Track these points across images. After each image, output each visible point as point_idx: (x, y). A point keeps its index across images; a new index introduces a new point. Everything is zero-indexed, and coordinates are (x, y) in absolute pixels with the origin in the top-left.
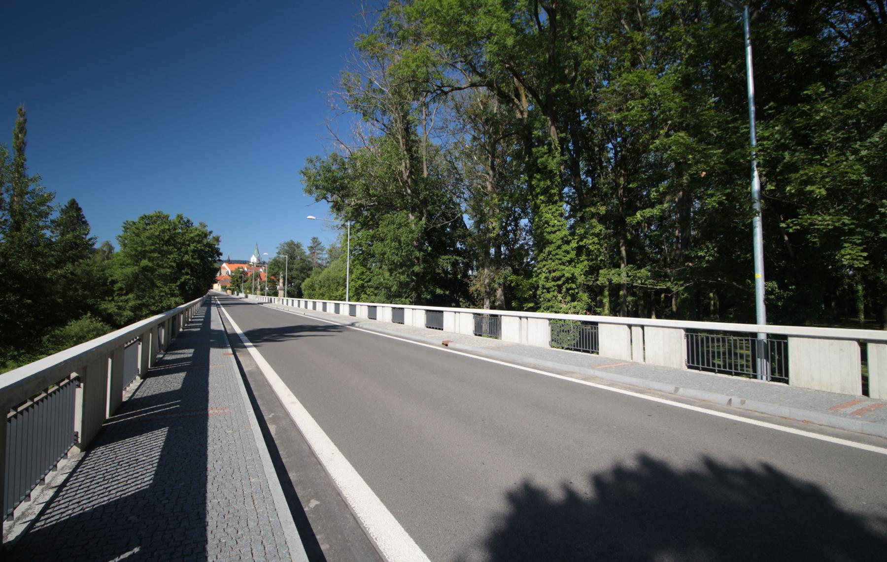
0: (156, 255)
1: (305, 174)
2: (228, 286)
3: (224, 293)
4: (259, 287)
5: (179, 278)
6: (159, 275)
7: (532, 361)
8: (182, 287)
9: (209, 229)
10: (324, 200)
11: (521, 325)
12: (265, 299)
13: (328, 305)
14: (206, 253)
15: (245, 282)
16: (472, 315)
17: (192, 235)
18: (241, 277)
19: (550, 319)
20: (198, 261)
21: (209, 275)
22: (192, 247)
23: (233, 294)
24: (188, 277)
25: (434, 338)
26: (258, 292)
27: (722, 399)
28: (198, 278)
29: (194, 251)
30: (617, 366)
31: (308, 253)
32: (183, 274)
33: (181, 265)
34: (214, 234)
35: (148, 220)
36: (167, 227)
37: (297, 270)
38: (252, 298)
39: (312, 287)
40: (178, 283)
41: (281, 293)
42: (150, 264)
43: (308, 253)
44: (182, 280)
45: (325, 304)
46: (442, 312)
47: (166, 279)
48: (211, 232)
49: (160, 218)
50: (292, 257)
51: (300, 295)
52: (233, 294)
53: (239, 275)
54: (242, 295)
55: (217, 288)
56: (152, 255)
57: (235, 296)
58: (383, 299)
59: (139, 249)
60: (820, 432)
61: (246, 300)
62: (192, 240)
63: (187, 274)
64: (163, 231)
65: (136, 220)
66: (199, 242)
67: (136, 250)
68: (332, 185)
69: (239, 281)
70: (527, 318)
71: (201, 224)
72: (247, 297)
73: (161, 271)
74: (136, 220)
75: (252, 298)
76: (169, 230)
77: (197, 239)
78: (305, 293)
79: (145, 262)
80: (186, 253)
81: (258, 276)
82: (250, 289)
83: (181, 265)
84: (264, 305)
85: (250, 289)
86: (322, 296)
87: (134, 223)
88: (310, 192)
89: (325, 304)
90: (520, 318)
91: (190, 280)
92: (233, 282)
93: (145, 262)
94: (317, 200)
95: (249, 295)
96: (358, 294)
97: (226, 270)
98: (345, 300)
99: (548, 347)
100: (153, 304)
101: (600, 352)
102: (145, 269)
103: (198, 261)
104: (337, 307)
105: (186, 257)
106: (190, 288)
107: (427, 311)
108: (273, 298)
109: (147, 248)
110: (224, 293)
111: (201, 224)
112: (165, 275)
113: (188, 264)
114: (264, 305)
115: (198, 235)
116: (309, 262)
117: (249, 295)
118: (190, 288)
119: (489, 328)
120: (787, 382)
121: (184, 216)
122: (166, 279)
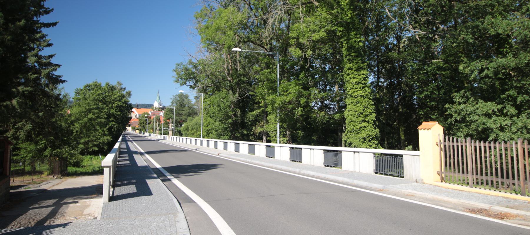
0: (96, 111)
1: (175, 71)
2: (137, 127)
3: (134, 133)
4: (158, 129)
5: (107, 124)
6: (98, 123)
7: (258, 162)
8: (110, 129)
9: (123, 86)
10: (185, 85)
11: (354, 157)
12: (162, 137)
13: (218, 143)
14: (123, 107)
15: (149, 124)
16: (322, 151)
17: (116, 96)
18: (146, 120)
19: (374, 153)
20: (119, 113)
21: (125, 121)
22: (116, 105)
23: (140, 133)
24: (113, 123)
25: (294, 169)
26: (157, 132)
27: (380, 186)
28: (119, 124)
29: (117, 107)
30: (351, 174)
31: (194, 101)
32: (110, 121)
33: (109, 116)
34: (127, 90)
35: (88, 87)
36: (101, 92)
37: (185, 114)
38: (154, 136)
39: (187, 129)
40: (108, 127)
41: (170, 133)
42: (94, 117)
43: (194, 101)
44: (110, 125)
45: (216, 142)
46: (301, 149)
47: (102, 125)
48: (125, 89)
49: (97, 86)
50: (182, 105)
51: (181, 135)
52: (140, 133)
53: (145, 119)
54: (147, 134)
55: (129, 129)
56: (94, 111)
57: (142, 135)
58: (215, 136)
59: (87, 107)
60: (394, 195)
61: (150, 138)
62: (115, 100)
63: (112, 121)
64: (99, 95)
65: (82, 88)
66: (120, 101)
67: (86, 109)
68: (188, 76)
69: (145, 123)
70: (359, 152)
71: (118, 83)
72: (150, 135)
73: (99, 120)
74: (82, 88)
75: (154, 136)
76: (102, 93)
77: (118, 99)
78: (183, 133)
79: (90, 116)
80: (112, 108)
81: (158, 119)
82: (153, 129)
83: (109, 116)
84: (161, 141)
85: (153, 129)
86: (193, 135)
87: (81, 90)
88: (177, 81)
89: (216, 142)
90: (355, 152)
91: (114, 125)
92: (140, 124)
93: (90, 116)
94: (181, 85)
95: (152, 134)
96: (208, 134)
97: (135, 114)
98: (200, 137)
99: (289, 160)
100: (95, 141)
101: (303, 161)
102: (91, 119)
103: (119, 113)
104: (237, 146)
105: (112, 111)
106: (114, 130)
107: (249, 144)
108: (166, 136)
109: (92, 107)
110: (134, 133)
111: (118, 83)
112: (101, 122)
113: (113, 115)
114: (161, 141)
115: (119, 96)
116: (194, 109)
117: (152, 134)
118: (114, 130)
119: (333, 161)
120: (403, 177)
121: (110, 84)
122: (102, 125)
